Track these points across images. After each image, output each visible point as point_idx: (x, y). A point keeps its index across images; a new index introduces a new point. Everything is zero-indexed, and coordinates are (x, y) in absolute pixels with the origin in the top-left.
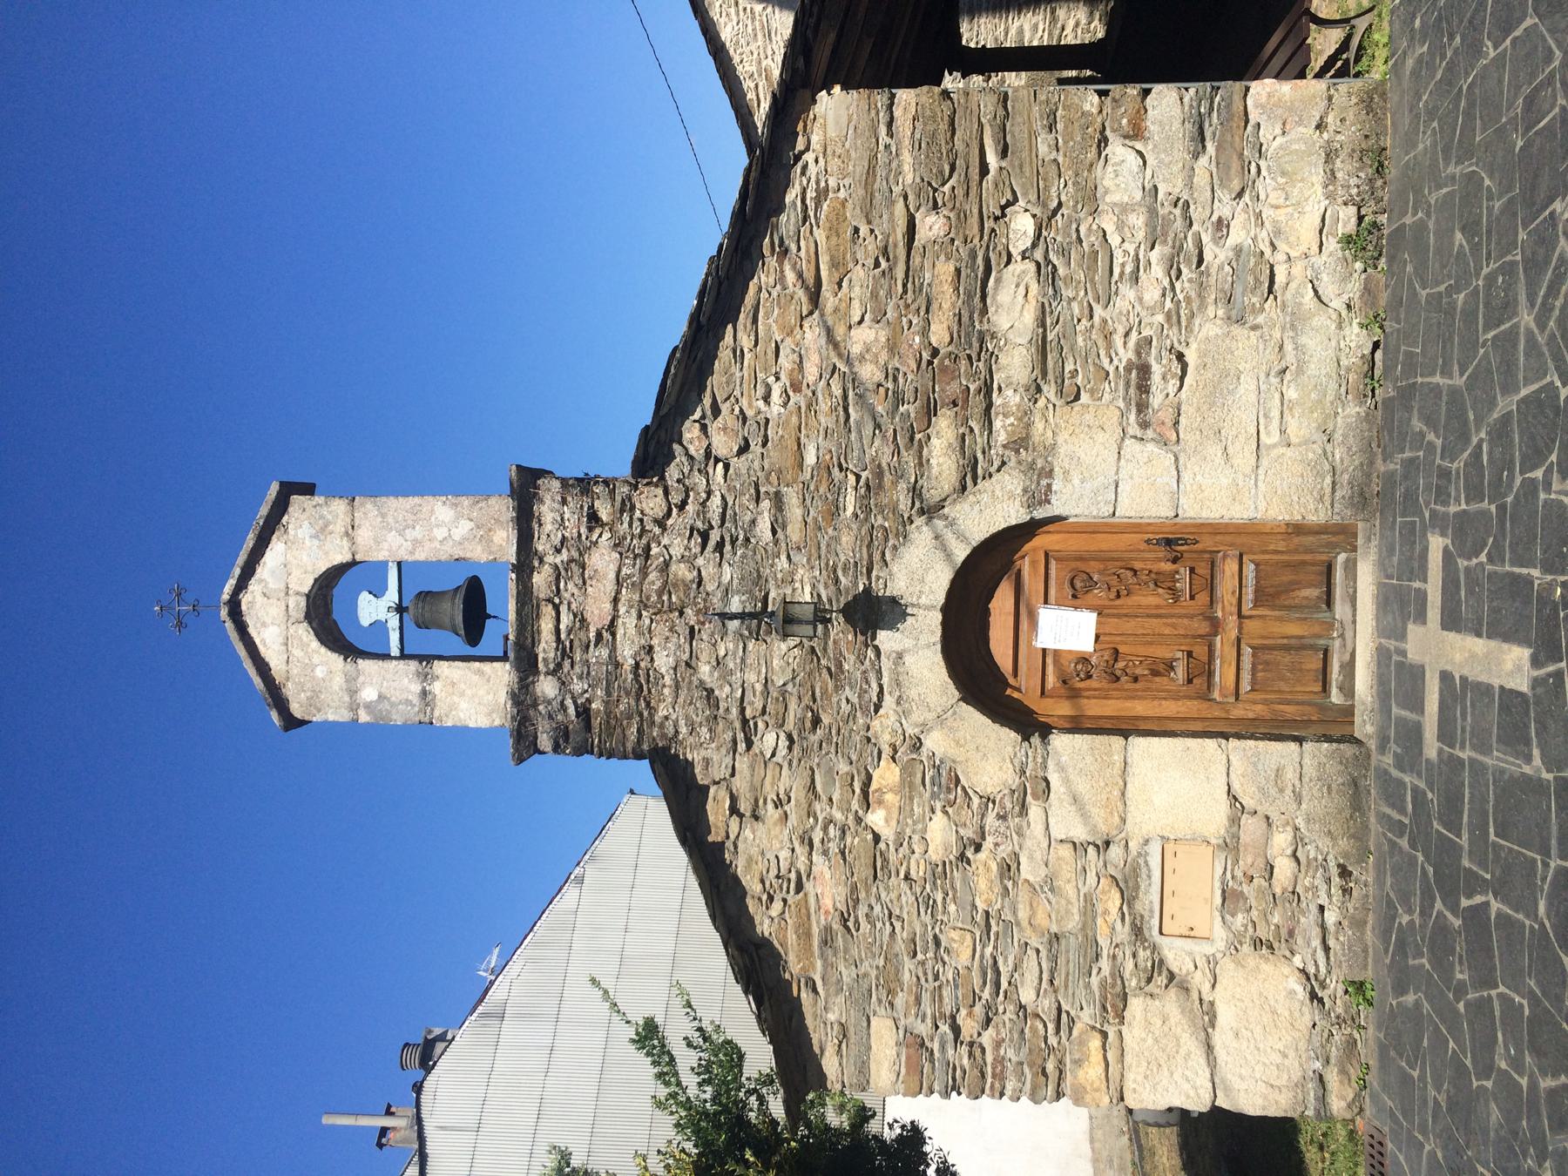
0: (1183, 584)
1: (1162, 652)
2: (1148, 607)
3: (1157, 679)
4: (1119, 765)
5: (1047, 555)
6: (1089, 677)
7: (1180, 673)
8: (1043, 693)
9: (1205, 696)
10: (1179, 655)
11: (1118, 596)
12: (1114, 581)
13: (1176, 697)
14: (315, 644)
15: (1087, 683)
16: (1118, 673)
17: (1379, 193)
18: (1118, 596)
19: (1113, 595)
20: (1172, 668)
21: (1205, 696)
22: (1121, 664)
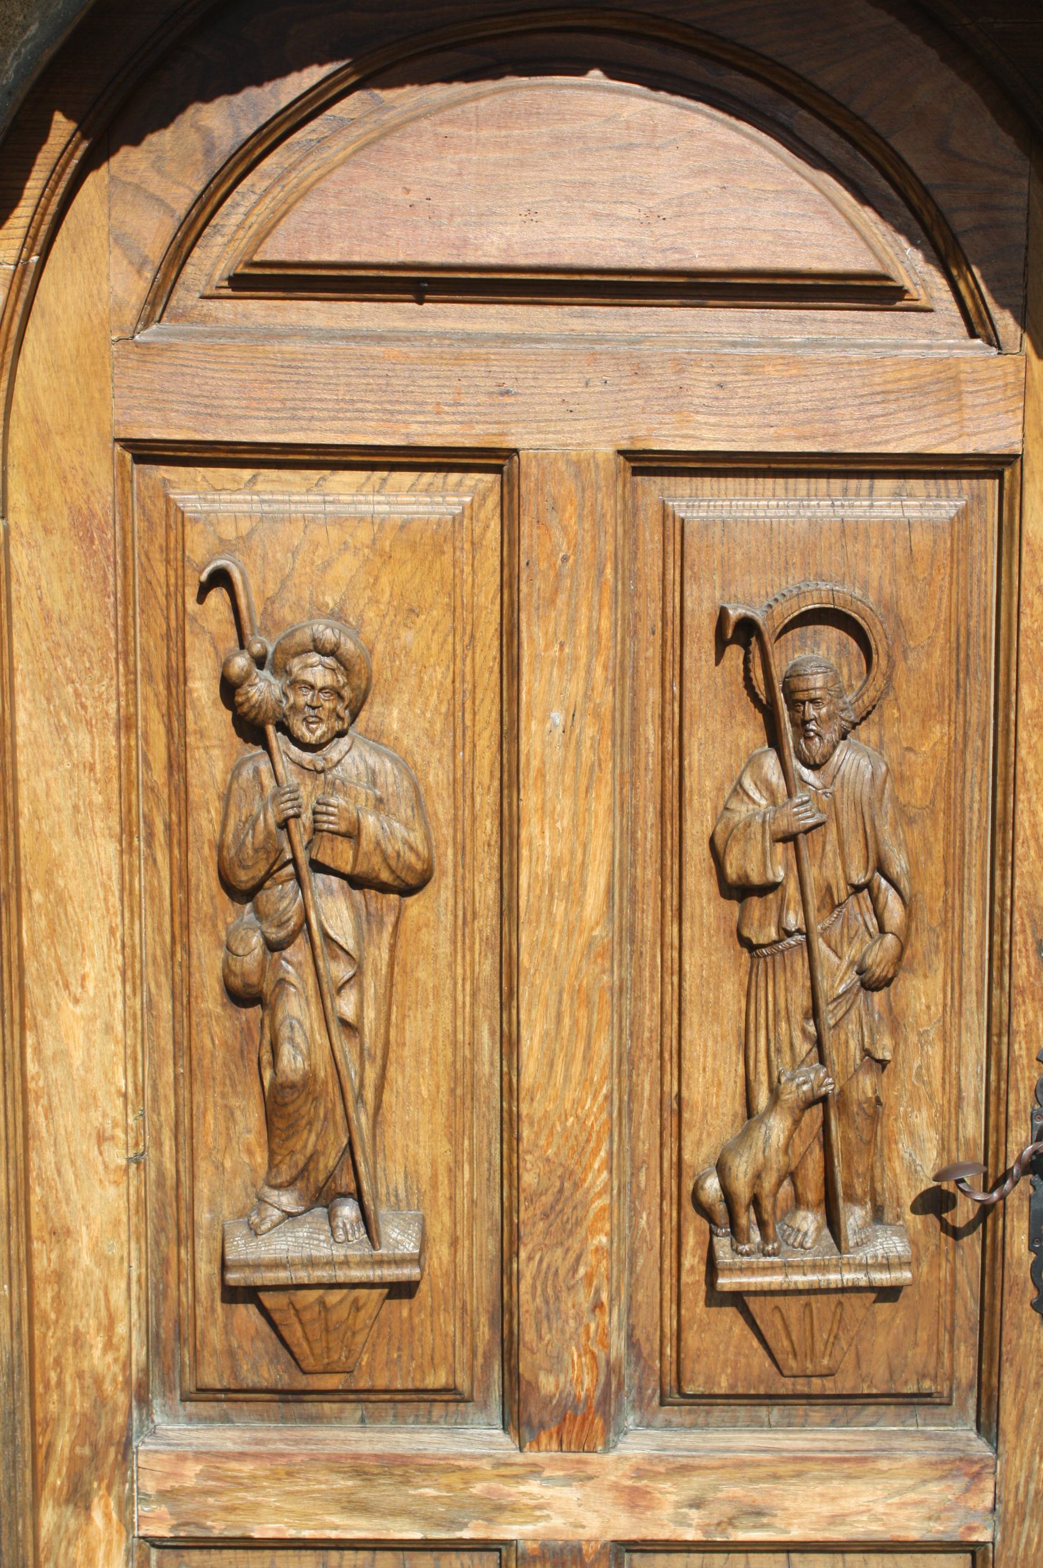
0: (797, 1259)
1: (415, 1141)
2: (455, 855)
3: (250, 1118)
4: (256, 1060)
5: (995, 466)
6: (251, 728)
7: (292, 1243)
8: (147, 452)
9: (174, 1370)
10: (399, 1237)
11: (738, 891)
12: (834, 865)
13: (168, 1216)
14: (859, 207)
15: (211, 718)
16: (282, 898)
17: (347, 1006)
18: (738, 891)
19: (747, 862)
20: (323, 1198)
21: (174, 1370)
22: (336, 912)
